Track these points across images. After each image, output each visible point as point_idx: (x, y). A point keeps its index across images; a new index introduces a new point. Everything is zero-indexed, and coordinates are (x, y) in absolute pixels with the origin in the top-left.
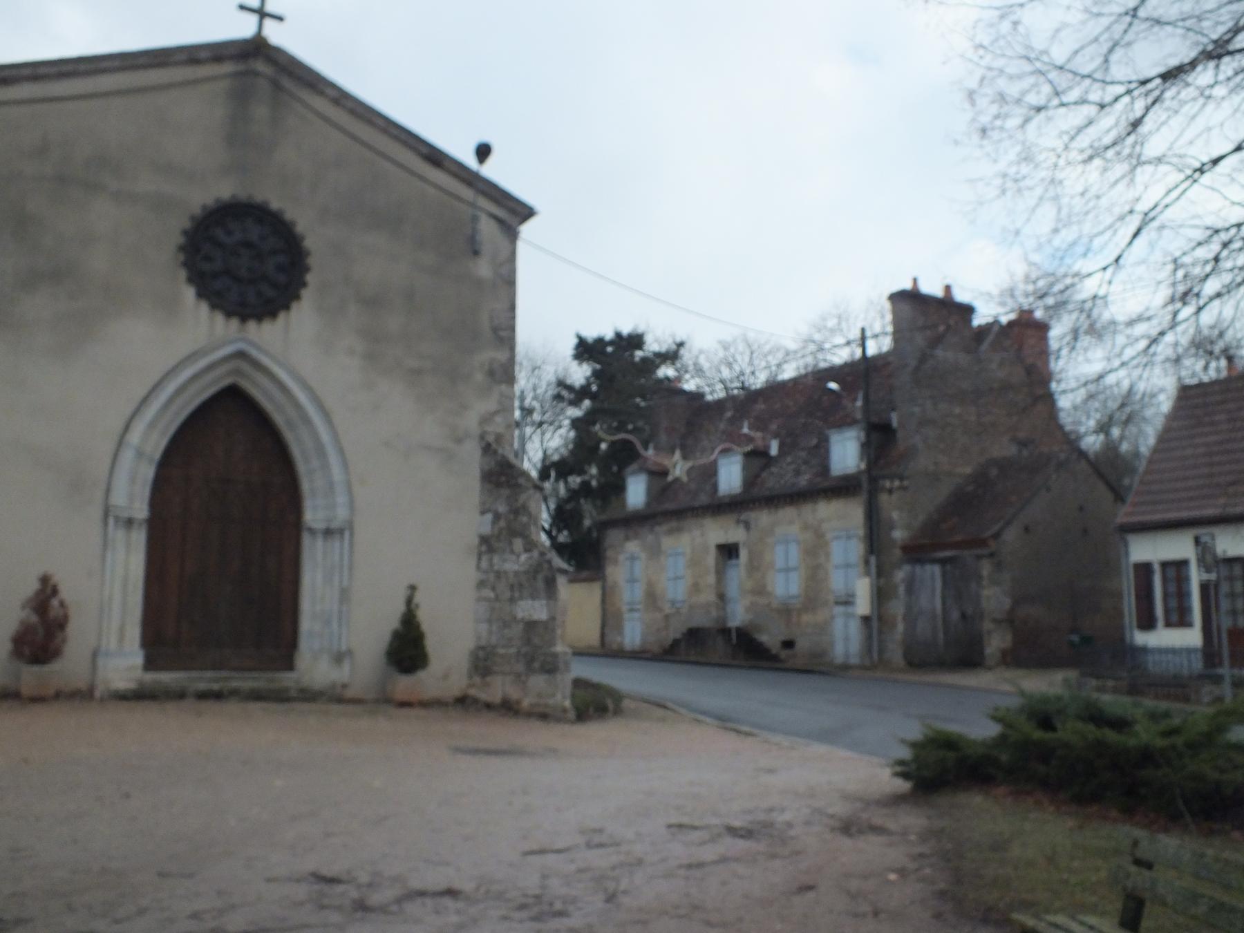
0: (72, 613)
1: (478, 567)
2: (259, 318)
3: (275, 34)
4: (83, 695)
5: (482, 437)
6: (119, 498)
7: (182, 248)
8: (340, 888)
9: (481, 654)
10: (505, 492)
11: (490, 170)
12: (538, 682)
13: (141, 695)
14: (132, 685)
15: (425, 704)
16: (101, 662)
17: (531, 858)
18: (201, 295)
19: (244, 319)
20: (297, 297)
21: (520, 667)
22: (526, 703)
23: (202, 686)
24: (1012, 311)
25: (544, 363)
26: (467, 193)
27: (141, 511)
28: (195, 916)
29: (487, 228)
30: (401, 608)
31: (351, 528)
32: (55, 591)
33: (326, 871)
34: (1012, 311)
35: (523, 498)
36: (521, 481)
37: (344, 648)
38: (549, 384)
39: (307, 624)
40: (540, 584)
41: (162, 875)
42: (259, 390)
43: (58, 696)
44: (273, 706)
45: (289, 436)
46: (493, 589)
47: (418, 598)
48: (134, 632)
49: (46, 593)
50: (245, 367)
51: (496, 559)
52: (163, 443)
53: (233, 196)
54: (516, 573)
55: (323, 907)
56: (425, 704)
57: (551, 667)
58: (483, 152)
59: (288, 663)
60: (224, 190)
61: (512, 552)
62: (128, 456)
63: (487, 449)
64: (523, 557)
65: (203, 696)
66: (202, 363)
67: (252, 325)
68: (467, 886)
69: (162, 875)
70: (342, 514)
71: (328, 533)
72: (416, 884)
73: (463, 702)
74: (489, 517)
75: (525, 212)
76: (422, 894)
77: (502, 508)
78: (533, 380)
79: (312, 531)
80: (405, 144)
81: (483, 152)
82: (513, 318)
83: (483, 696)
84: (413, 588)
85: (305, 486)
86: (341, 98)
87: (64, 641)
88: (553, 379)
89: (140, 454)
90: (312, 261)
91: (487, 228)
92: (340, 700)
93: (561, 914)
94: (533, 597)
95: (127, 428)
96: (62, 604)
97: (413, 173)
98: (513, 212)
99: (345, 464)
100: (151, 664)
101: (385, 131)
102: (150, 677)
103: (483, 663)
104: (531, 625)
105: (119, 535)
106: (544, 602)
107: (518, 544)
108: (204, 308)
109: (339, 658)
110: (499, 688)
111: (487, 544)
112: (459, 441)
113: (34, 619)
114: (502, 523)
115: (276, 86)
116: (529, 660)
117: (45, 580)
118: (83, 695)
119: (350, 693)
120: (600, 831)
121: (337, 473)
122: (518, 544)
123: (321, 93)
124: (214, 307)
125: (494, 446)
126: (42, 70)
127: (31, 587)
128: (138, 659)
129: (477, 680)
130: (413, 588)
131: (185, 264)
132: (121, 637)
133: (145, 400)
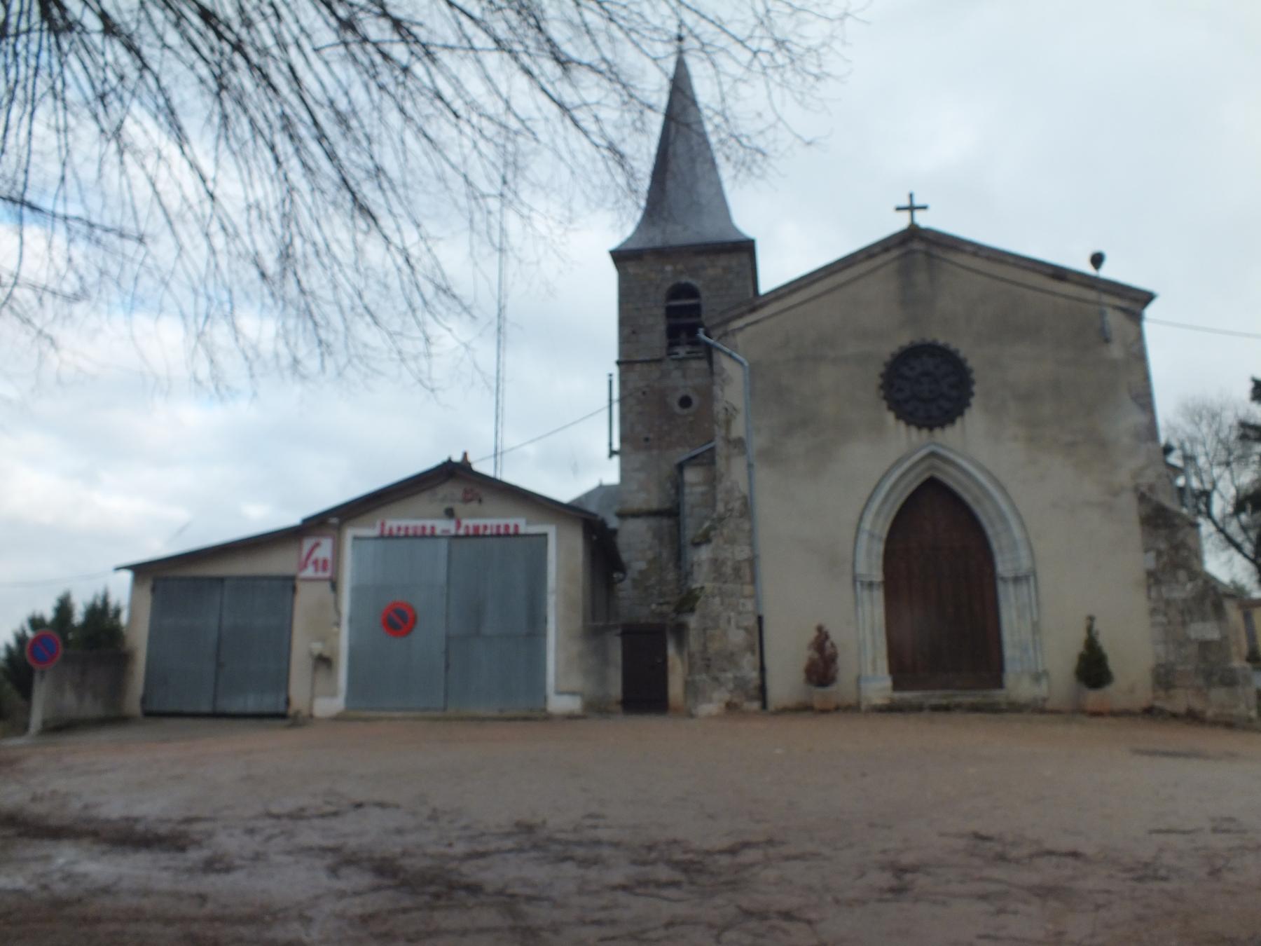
0: (840, 650)
1: (1149, 598)
2: (942, 425)
3: (923, 220)
4: (851, 709)
5: (1136, 489)
6: (862, 569)
7: (882, 387)
8: (988, 844)
9: (1162, 671)
10: (1163, 532)
11: (1107, 272)
12: (1219, 695)
13: (891, 709)
14: (886, 702)
15: (1115, 714)
16: (863, 685)
17: (1154, 836)
18: (899, 417)
19: (931, 428)
20: (968, 405)
21: (1200, 681)
22: (1210, 713)
23: (934, 701)
25: (1222, 409)
26: (1091, 295)
27: (878, 576)
28: (884, 852)
29: (1114, 319)
30: (1082, 635)
31: (1034, 573)
32: (827, 637)
33: (983, 832)
35: (1180, 535)
36: (1177, 521)
37: (1040, 669)
38: (1230, 427)
39: (1009, 652)
41: (872, 825)
43: (837, 709)
44: (988, 716)
45: (977, 509)
46: (1166, 614)
47: (1098, 626)
48: (883, 664)
49: (821, 641)
50: (937, 462)
51: (1164, 589)
52: (887, 527)
53: (912, 343)
54: (1185, 601)
55: (972, 855)
56: (1115, 714)
57: (1230, 681)
58: (1097, 260)
59: (998, 682)
60: (904, 339)
61: (1177, 582)
62: (864, 538)
63: (1142, 498)
65: (936, 708)
66: (906, 465)
67: (938, 432)
68: (1089, 849)
69: (872, 825)
70: (1025, 564)
71: (1017, 580)
72: (1048, 845)
73: (1150, 712)
74: (1152, 555)
75: (1146, 298)
76: (1050, 853)
77: (1163, 546)
78: (1215, 426)
79: (1004, 580)
80: (1034, 270)
81: (1097, 260)
83: (1168, 707)
84: (1091, 619)
85: (995, 545)
86: (978, 250)
87: (837, 671)
88: (1235, 423)
89: (872, 536)
90: (974, 376)
91: (1114, 319)
92: (1042, 711)
93: (1165, 879)
94: (1204, 619)
95: (861, 519)
96: (833, 645)
97: (1042, 291)
98: (1135, 300)
100: (897, 686)
102: (898, 695)
103: (1164, 678)
104: (1205, 645)
105: (865, 595)
107: (1182, 575)
108: (902, 425)
109: (1037, 677)
110: (1181, 700)
111: (1154, 578)
112: (1116, 494)
113: (816, 656)
114: (1165, 559)
115: (929, 255)
116: (1208, 675)
117: (820, 629)
118: (851, 709)
119: (1049, 706)
120: (1231, 820)
121: (1017, 531)
122: (1182, 575)
123: (963, 251)
124: (908, 423)
125: (1148, 494)
126: (781, 292)
127: (813, 634)
128: (887, 682)
129: (1161, 693)
130: (1091, 619)
131: (885, 398)
132: (875, 669)
133: (870, 498)
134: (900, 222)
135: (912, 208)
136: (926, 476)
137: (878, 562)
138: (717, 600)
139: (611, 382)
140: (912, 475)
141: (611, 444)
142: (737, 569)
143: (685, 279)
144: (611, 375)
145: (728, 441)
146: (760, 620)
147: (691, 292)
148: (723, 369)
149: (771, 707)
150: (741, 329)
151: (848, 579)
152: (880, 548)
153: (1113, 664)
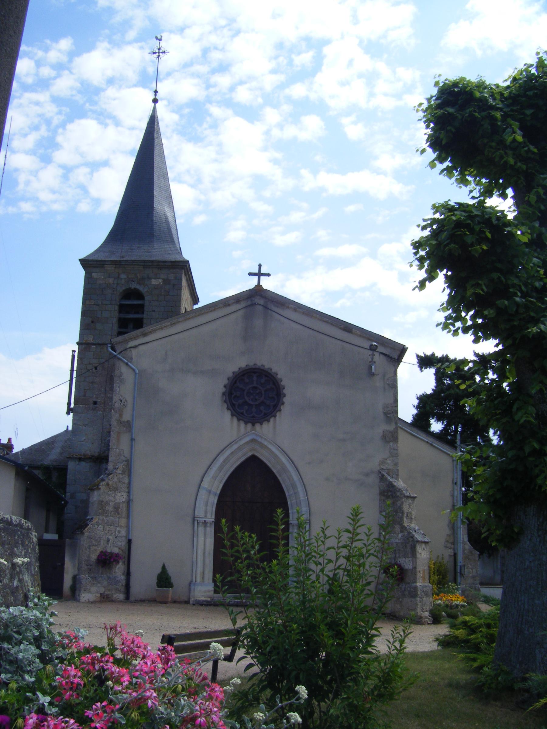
3: (267, 284)
6: (200, 512)
7: (224, 394)
24: (210, 598)
34: (210, 598)
40: (409, 549)
42: (264, 456)
60: (242, 363)
62: (203, 494)
63: (382, 478)
64: (400, 535)
66: (235, 447)
67: (258, 426)
82: (397, 406)
99: (212, 510)
101: (295, 310)
102: (218, 597)
106: (410, 559)
107: (397, 528)
115: (266, 307)
128: (211, 587)
134: (251, 283)
135: (259, 275)
136: (250, 454)
137: (212, 510)
138: (101, 527)
139: (73, 357)
140: (240, 454)
141: (69, 404)
142: (117, 508)
143: (134, 286)
144: (74, 351)
145: (120, 422)
146: (130, 542)
147: (139, 295)
148: (121, 374)
149: (132, 598)
150: (135, 347)
151: (190, 519)
152: (214, 500)
153: (174, 580)
